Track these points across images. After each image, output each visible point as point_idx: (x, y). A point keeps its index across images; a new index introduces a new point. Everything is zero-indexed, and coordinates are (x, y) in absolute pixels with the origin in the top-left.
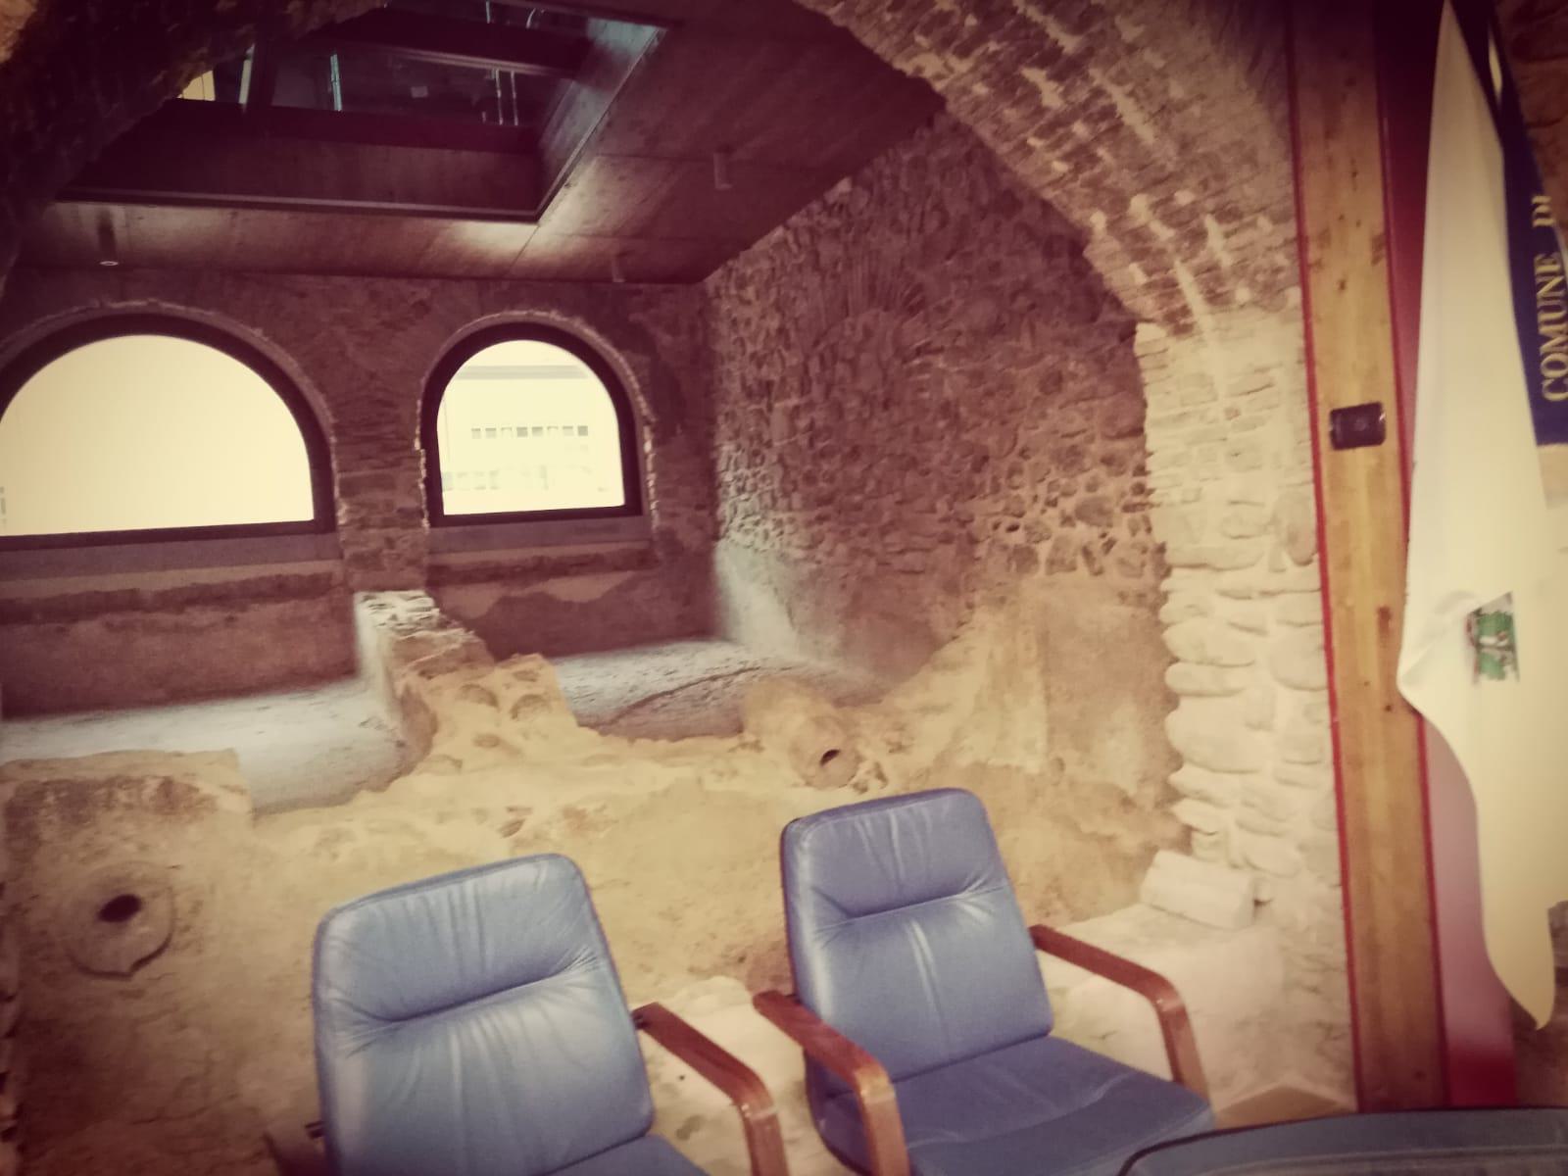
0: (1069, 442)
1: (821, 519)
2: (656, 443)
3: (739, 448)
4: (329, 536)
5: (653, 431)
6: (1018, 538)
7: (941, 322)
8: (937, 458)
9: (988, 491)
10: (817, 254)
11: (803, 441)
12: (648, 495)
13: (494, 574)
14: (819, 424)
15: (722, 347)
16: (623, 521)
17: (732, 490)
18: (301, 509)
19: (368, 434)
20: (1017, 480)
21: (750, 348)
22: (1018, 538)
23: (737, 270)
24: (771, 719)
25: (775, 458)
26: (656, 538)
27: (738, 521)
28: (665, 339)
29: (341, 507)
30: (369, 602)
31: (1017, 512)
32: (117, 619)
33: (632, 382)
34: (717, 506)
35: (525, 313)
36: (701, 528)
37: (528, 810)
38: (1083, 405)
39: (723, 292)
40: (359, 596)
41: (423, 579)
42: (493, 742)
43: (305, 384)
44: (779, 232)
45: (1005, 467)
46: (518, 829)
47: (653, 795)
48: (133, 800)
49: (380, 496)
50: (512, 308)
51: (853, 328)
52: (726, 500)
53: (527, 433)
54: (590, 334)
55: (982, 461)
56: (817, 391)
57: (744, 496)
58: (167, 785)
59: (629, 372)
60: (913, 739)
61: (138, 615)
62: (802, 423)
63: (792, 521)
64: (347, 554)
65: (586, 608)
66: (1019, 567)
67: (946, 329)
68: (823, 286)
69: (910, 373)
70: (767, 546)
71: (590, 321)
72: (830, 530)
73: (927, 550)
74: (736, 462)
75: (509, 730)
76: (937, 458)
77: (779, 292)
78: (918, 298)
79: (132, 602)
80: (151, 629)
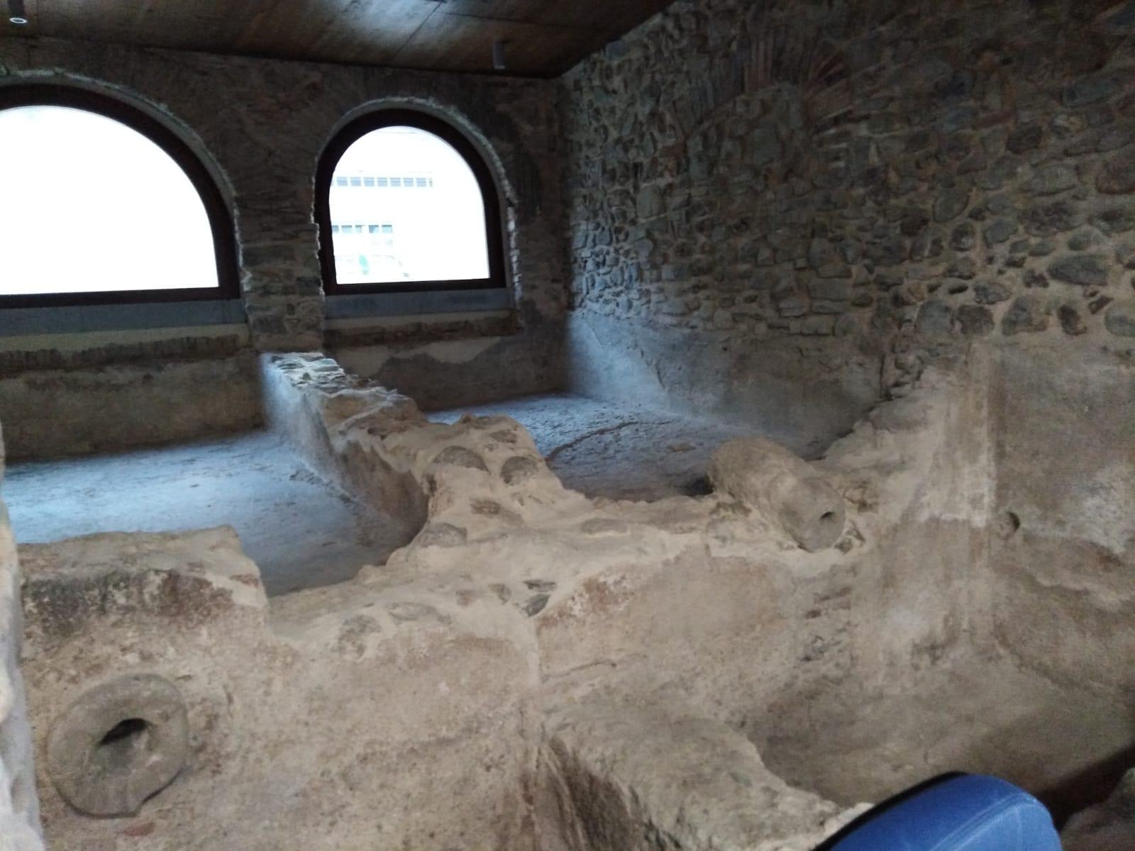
0: (1048, 201)
1: (697, 288)
2: (518, 224)
3: (598, 226)
4: (233, 302)
5: (517, 211)
6: (968, 298)
7: (868, 88)
8: (851, 226)
9: (926, 253)
10: (705, 39)
11: (674, 216)
12: (511, 269)
13: (379, 338)
14: (696, 199)
15: (579, 137)
16: (489, 292)
17: (590, 265)
18: (207, 277)
19: (268, 206)
20: (967, 241)
21: (614, 134)
22: (968, 298)
23: (602, 62)
24: (756, 481)
25: (642, 234)
26: (518, 307)
27: (595, 292)
28: (527, 129)
29: (245, 275)
30: (278, 362)
31: (967, 274)
32: (40, 377)
33: (498, 166)
34: (572, 280)
35: (406, 99)
36: (556, 298)
37: (552, 585)
38: (1071, 161)
39: (584, 83)
40: (266, 357)
41: (319, 342)
42: (489, 508)
43: (209, 159)
44: (657, 20)
45: (948, 230)
46: (543, 606)
47: (666, 563)
48: (133, 602)
49: (280, 265)
50: (395, 95)
51: (747, 104)
52: (581, 274)
53: (407, 209)
54: (462, 121)
55: (914, 224)
56: (696, 169)
57: (602, 271)
58: (172, 579)
59: (496, 157)
60: (876, 496)
61: (59, 373)
62: (677, 199)
63: (661, 290)
64: (251, 319)
65: (462, 369)
66: (964, 330)
67: (875, 96)
68: (711, 67)
69: (820, 144)
70: (632, 313)
71: (463, 110)
72: (708, 298)
73: (836, 314)
74: (594, 241)
75: (502, 493)
76: (851, 226)
77: (653, 78)
78: (839, 67)
79: (53, 361)
80: (74, 386)
